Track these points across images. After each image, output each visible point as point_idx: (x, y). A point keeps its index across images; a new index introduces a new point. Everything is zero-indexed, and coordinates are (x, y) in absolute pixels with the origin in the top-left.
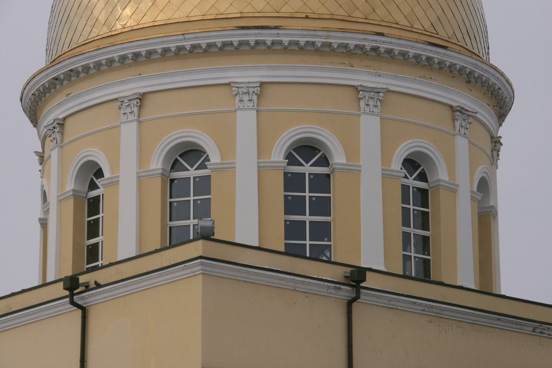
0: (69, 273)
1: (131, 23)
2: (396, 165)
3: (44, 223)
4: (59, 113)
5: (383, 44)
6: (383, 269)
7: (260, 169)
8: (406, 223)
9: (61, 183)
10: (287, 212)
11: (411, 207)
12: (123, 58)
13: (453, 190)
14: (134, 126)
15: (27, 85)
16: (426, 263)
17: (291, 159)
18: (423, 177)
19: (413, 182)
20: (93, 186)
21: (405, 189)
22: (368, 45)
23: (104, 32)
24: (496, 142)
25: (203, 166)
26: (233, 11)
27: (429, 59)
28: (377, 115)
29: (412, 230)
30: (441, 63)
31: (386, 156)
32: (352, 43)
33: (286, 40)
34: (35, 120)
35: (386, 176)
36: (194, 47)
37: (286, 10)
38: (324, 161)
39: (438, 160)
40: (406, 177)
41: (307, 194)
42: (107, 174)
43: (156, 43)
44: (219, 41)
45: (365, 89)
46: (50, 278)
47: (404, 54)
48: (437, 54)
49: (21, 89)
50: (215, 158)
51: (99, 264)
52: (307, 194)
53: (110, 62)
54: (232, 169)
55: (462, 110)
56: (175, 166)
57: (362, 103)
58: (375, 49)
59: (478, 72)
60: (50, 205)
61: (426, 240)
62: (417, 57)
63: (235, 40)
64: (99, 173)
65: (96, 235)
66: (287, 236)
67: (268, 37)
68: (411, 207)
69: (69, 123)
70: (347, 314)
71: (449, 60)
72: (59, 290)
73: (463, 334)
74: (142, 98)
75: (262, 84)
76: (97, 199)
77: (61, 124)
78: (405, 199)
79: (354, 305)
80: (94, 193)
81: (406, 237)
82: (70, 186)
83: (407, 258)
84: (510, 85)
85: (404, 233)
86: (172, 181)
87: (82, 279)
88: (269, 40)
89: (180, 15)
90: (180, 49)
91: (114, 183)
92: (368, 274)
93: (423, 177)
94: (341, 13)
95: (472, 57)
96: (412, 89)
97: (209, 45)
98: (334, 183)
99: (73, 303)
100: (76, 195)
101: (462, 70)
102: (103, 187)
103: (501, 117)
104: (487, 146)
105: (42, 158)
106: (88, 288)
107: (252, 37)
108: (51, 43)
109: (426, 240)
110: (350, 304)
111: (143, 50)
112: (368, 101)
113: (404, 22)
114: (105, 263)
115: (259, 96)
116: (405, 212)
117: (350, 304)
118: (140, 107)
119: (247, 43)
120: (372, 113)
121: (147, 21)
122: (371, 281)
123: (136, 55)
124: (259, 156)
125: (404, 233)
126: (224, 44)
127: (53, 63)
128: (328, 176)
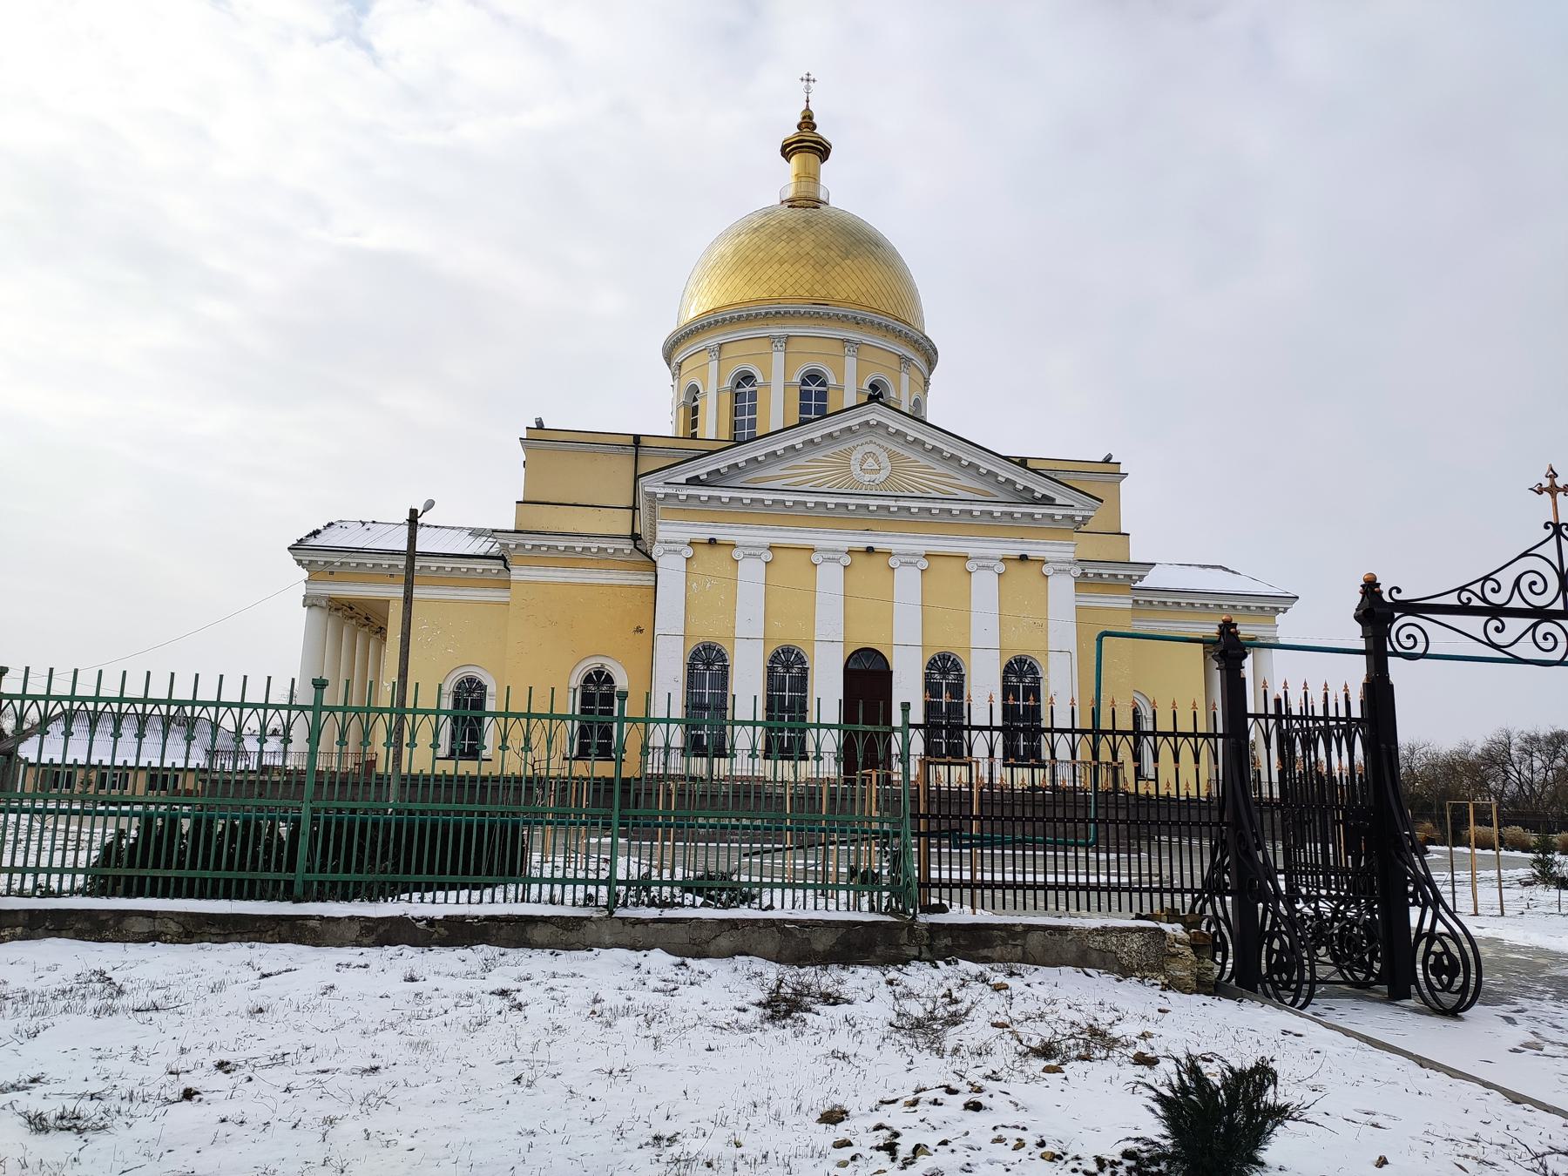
2: (866, 386)
4: (678, 360)
15: (544, 533)
17: (804, 382)
20: (695, 400)
24: (927, 383)
25: (753, 385)
28: (673, 748)
31: (859, 380)
38: (824, 384)
42: (701, 392)
43: (703, 320)
45: (848, 341)
50: (760, 379)
56: (739, 385)
57: (846, 349)
65: (696, 427)
73: (624, 1007)
86: (736, 394)
102: (789, 207)
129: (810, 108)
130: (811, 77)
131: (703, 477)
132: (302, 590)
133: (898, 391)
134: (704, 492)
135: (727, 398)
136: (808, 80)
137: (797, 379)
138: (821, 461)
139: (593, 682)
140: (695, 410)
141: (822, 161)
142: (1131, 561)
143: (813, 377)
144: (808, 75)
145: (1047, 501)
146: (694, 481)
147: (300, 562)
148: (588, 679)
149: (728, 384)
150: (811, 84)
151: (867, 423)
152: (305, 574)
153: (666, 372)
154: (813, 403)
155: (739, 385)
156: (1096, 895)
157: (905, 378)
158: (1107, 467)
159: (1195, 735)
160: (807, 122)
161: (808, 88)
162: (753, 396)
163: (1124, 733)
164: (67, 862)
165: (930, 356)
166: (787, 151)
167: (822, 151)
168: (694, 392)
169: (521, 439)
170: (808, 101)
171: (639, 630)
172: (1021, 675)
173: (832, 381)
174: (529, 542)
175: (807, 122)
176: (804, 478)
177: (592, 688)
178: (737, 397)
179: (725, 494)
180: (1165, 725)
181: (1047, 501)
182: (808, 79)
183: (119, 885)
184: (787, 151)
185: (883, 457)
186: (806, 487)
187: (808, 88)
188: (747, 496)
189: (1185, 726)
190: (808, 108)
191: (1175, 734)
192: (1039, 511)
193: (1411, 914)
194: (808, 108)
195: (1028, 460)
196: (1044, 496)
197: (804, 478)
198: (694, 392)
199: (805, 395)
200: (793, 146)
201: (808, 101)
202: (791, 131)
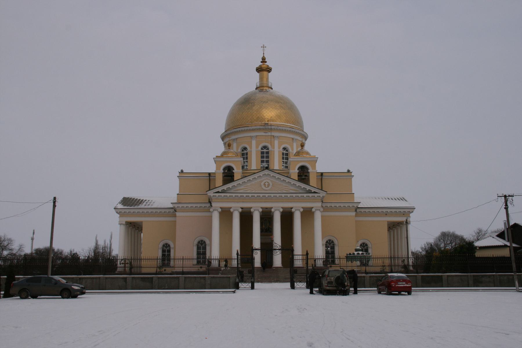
11: (285, 156)
17: (262, 149)
18: (287, 151)
19: (285, 152)
25: (246, 151)
29: (285, 160)
31: (279, 148)
34: (223, 141)
35: (279, 152)
38: (268, 149)
39: (334, 240)
40: (283, 151)
41: (265, 155)
49: (308, 134)
51: (234, 170)
52: (265, 155)
54: (251, 151)
56: (243, 151)
68: (285, 156)
84: (307, 134)
85: (283, 157)
93: (287, 151)
96: (405, 250)
103: (306, 140)
109: (287, 153)
112: (157, 315)
115: (256, 138)
118: (236, 140)
125: (283, 157)
127: (225, 131)
129: (265, 56)
130: (264, 46)
131: (220, 191)
132: (118, 220)
134: (223, 195)
136: (264, 47)
137: (260, 148)
139: (165, 246)
141: (269, 73)
142: (252, 169)
143: (265, 147)
144: (264, 45)
145: (315, 192)
146: (218, 192)
147: (117, 212)
150: (265, 48)
151: (265, 174)
152: (119, 215)
153: (222, 143)
158: (348, 174)
159: (387, 258)
160: (264, 60)
161: (264, 49)
162: (247, 154)
167: (269, 70)
169: (178, 176)
170: (264, 54)
172: (166, 247)
174: (180, 205)
175: (264, 60)
176: (250, 188)
177: (165, 248)
179: (228, 195)
181: (315, 192)
182: (264, 47)
183: (232, 196)
186: (249, 192)
187: (264, 49)
188: (234, 195)
189: (386, 257)
190: (264, 57)
191: (385, 258)
192: (311, 195)
195: (323, 173)
196: (314, 192)
197: (250, 188)
199: (262, 153)
200: (259, 70)
201: (264, 54)
202: (258, 64)
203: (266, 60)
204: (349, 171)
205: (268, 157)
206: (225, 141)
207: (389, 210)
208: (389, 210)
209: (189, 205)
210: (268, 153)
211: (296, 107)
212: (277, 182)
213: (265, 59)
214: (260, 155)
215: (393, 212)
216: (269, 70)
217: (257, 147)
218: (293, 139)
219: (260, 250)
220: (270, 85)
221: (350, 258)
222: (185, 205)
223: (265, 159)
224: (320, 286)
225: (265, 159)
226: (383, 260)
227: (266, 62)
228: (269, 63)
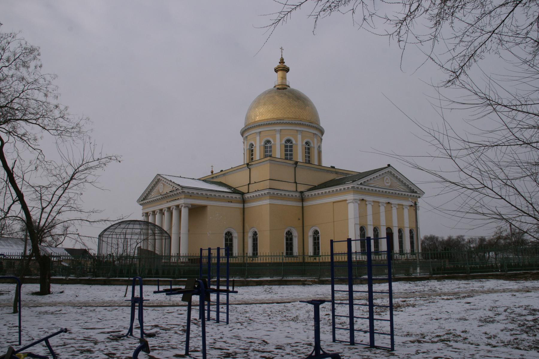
0: (248, 162)
1: (258, 120)
2: (304, 143)
3: (244, 154)
4: (246, 135)
5: (301, 122)
6: (302, 161)
7: (280, 144)
8: (306, 153)
9: (247, 146)
10: (285, 152)
12: (257, 125)
13: (314, 148)
14: (259, 137)
16: (309, 160)
17: (286, 142)
19: (307, 146)
21: (306, 147)
22: (299, 123)
23: (254, 121)
24: (321, 139)
25: (270, 144)
26: (276, 117)
27: (310, 125)
29: (307, 155)
30: (312, 126)
32: (296, 122)
33: (285, 122)
34: (242, 136)
35: (302, 145)
36: (269, 123)
37: (285, 117)
38: (292, 143)
42: (254, 145)
44: (273, 122)
46: (245, 163)
47: (305, 124)
48: (311, 124)
50: (273, 142)
52: (289, 148)
53: (255, 126)
55: (315, 134)
56: (266, 144)
58: (300, 123)
59: (318, 127)
60: (108, 336)
61: (309, 156)
62: (307, 125)
63: (276, 122)
64: (253, 145)
66: (285, 156)
67: (282, 121)
69: (248, 137)
70: (393, 232)
71: (313, 125)
72: (246, 165)
74: (260, 132)
75: (281, 130)
76: (253, 158)
77: (247, 137)
78: (306, 149)
79: (296, 168)
80: (252, 149)
81: (306, 156)
82: (248, 147)
83: (306, 160)
87: (249, 164)
88: (282, 122)
89: (266, 118)
90: (267, 124)
91: (255, 147)
92: (298, 163)
94: (294, 117)
95: (60, 188)
97: (272, 123)
98: (293, 146)
99: (248, 168)
100: (249, 149)
101: (315, 127)
103: (322, 135)
104: (320, 140)
105: (244, 143)
106: (250, 165)
107: (279, 121)
108: (245, 123)
109: (309, 156)
110: (295, 168)
111: (260, 124)
113: (305, 119)
114: (255, 160)
116: (306, 151)
117: (295, 168)
119: (278, 122)
120: (300, 134)
121: (261, 119)
122: (299, 164)
123: (259, 125)
124: (280, 142)
126: (274, 123)
127: (245, 126)
128: (292, 145)
133: (314, 144)
135: (262, 148)
137: (283, 142)
138: (377, 181)
140: (252, 151)
143: (288, 141)
147: (140, 204)
148: (226, 234)
149: (263, 143)
153: (241, 139)
154: (289, 148)
155: (266, 144)
156: (366, 291)
157: (315, 140)
160: (282, 61)
162: (271, 147)
163: (281, 256)
164: (139, 288)
165: (322, 132)
166: (276, 70)
167: (287, 70)
168: (252, 145)
171: (299, 219)
173: (294, 142)
175: (282, 61)
178: (266, 147)
180: (262, 255)
182: (282, 49)
184: (276, 70)
185: (389, 179)
186: (377, 186)
189: (267, 255)
190: (282, 57)
193: (369, 339)
194: (282, 57)
198: (252, 145)
202: (277, 64)
203: (284, 61)
204: (389, 165)
205: (291, 151)
206: (244, 136)
207: (195, 192)
208: (195, 192)
209: (287, 193)
210: (291, 147)
211: (311, 102)
212: (395, 181)
213: (283, 60)
214: (284, 148)
215: (199, 194)
216: (287, 70)
217: (281, 141)
218: (297, 130)
219: (386, 239)
220: (287, 84)
221: (384, 254)
222: (283, 193)
223: (289, 153)
224: (94, 259)
225: (289, 153)
226: (339, 258)
227: (284, 63)
228: (287, 64)
